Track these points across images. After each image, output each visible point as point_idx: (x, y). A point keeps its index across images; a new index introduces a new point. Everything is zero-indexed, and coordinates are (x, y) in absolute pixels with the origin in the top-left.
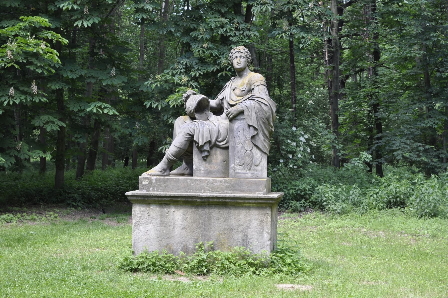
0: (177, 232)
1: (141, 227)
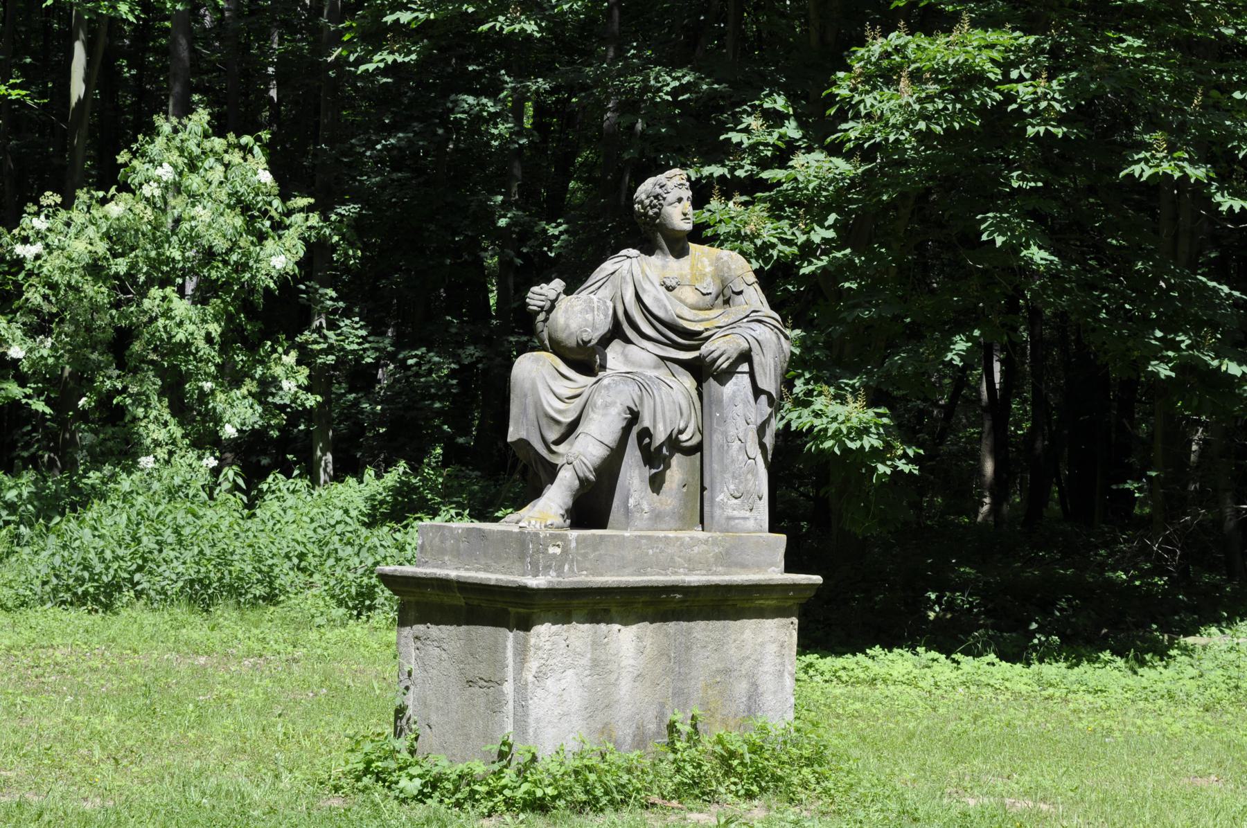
0: (625, 687)
1: (549, 682)
